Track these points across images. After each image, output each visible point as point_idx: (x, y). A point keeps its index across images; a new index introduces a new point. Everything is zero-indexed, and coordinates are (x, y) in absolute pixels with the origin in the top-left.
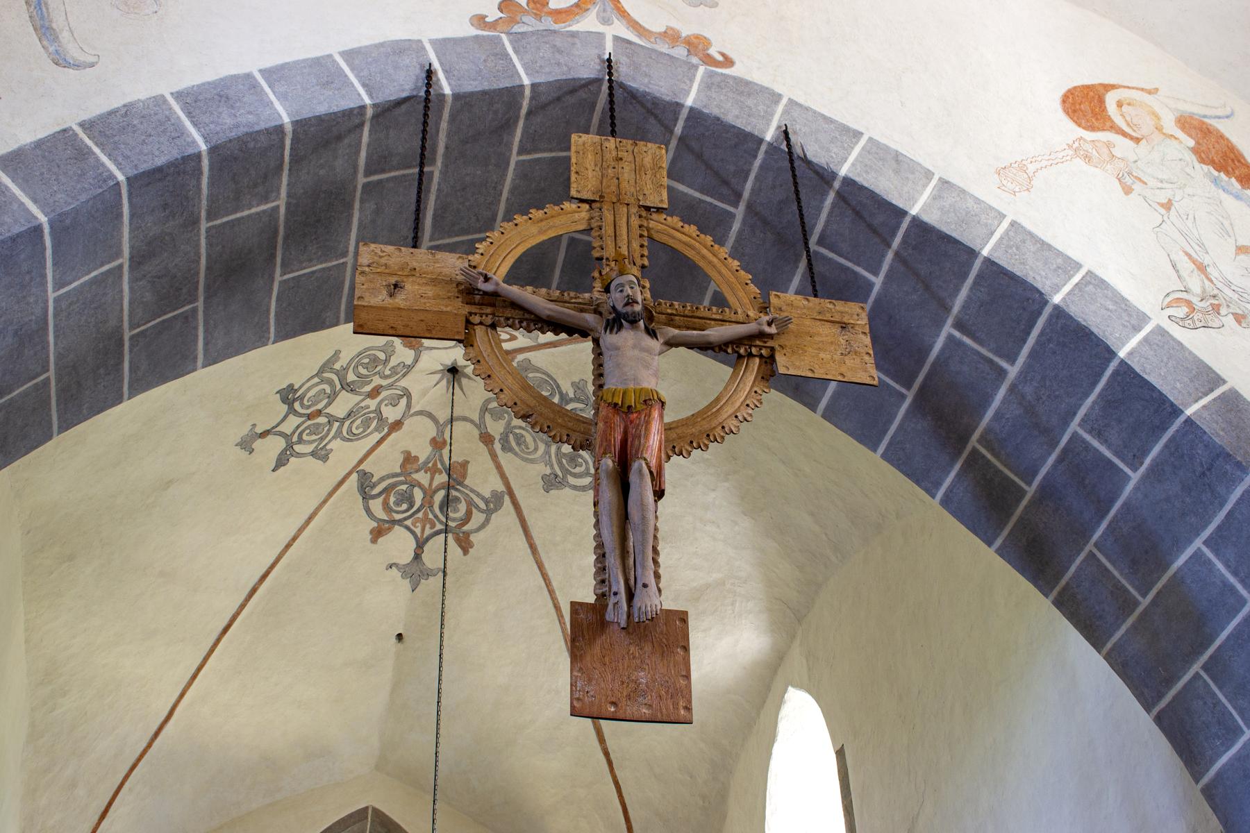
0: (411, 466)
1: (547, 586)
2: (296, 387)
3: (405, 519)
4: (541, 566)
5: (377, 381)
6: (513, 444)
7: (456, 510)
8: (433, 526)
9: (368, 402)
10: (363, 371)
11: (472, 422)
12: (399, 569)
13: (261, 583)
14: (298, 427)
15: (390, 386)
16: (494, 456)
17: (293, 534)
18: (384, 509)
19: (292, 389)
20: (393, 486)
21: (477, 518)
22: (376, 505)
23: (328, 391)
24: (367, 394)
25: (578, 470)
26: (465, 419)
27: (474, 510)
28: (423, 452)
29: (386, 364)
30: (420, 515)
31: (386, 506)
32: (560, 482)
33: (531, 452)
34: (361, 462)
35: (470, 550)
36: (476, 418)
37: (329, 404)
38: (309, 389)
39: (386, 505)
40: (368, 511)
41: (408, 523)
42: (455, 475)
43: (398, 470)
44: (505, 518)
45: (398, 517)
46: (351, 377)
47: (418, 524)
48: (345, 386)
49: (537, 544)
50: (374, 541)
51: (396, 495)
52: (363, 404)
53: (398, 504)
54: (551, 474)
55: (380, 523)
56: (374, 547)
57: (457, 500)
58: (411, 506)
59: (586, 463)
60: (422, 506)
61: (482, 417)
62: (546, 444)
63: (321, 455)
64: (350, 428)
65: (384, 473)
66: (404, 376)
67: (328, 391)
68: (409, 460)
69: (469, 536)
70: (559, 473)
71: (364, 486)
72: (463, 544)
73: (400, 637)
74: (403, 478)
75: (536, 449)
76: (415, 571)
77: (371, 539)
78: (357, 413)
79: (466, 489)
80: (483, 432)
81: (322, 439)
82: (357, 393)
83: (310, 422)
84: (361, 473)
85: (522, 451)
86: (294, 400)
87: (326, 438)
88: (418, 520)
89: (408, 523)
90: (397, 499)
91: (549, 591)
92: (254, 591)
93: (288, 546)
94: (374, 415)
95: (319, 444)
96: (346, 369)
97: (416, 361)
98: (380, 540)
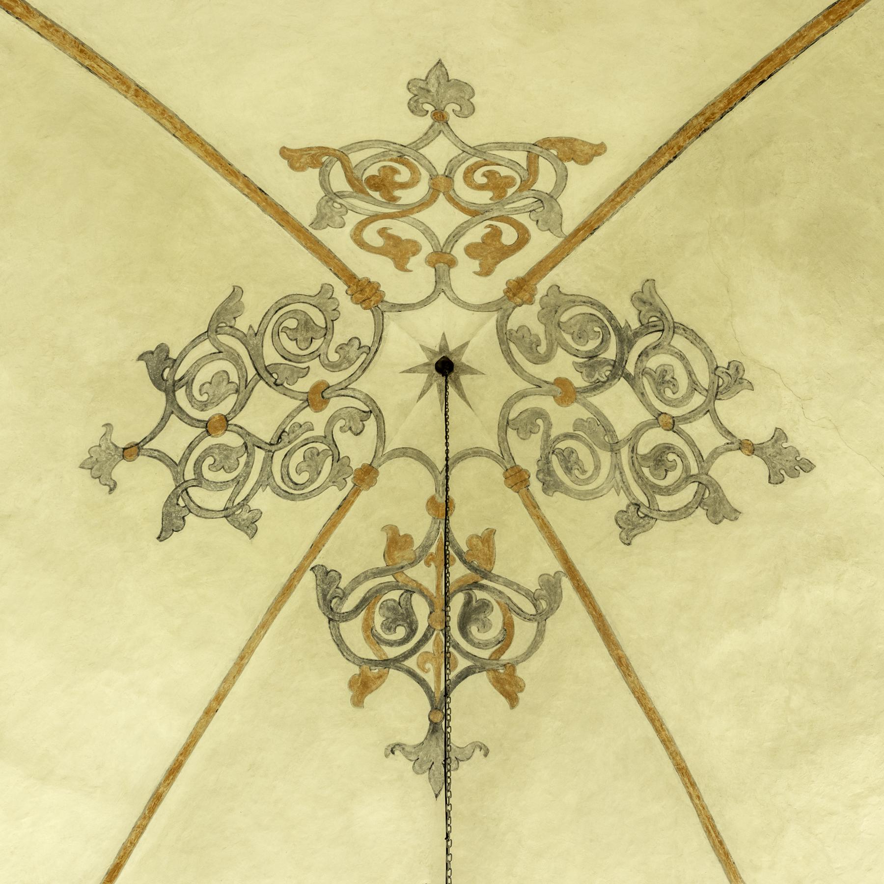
0: (400, 554)
1: (658, 731)
2: (174, 354)
3: (406, 656)
4: (641, 696)
5: (318, 374)
6: (560, 472)
7: (485, 626)
9: (307, 415)
10: (291, 347)
11: (488, 454)
12: (407, 755)
13: (169, 785)
14: (191, 448)
15: (343, 389)
16: (532, 506)
17: (215, 688)
18: (367, 638)
19: (167, 358)
21: (524, 631)
22: (352, 631)
24: (305, 397)
25: (673, 477)
26: (477, 452)
27: (516, 620)
29: (328, 337)
30: (429, 647)
31: (369, 633)
32: (646, 516)
33: (592, 476)
34: (316, 547)
35: (520, 695)
36: (494, 447)
37: (240, 406)
39: (369, 629)
40: (340, 643)
45: (393, 652)
47: (428, 666)
48: (265, 375)
49: (628, 655)
51: (385, 610)
52: (301, 418)
53: (389, 627)
54: (628, 506)
55: (365, 667)
56: (359, 713)
57: (485, 606)
58: (412, 632)
59: (681, 456)
60: (430, 629)
61: (503, 440)
62: (612, 451)
65: (358, 570)
66: (364, 368)
67: (234, 377)
68: (397, 543)
69: (514, 670)
70: (643, 499)
71: (328, 597)
72: (507, 687)
74: (389, 578)
75: (597, 468)
77: (352, 698)
78: (292, 436)
79: (496, 581)
80: (508, 466)
81: (239, 482)
82: (287, 392)
83: (209, 441)
84: (320, 573)
85: (576, 481)
87: (245, 480)
90: (387, 618)
91: (663, 741)
92: (157, 798)
93: (210, 712)
94: (324, 447)
95: (236, 494)
98: (368, 699)
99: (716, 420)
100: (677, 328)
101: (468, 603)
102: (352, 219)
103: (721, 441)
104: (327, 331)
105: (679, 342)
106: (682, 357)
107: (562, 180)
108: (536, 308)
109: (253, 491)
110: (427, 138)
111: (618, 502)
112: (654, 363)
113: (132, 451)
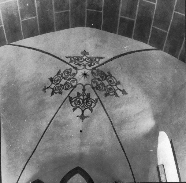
3: (79, 106)
5: (69, 77)
7: (89, 103)
8: (85, 108)
9: (68, 81)
10: (66, 75)
14: (54, 87)
16: (95, 91)
20: (76, 99)
21: (93, 105)
22: (73, 104)
23: (60, 79)
28: (81, 92)
30: (82, 105)
34: (69, 94)
37: (60, 82)
38: (55, 78)
39: (75, 104)
41: (80, 107)
42: (88, 96)
43: (77, 96)
44: (98, 104)
45: (78, 106)
46: (64, 76)
50: (74, 111)
52: (67, 82)
53: (77, 103)
56: (73, 112)
57: (89, 101)
58: (80, 103)
59: (113, 90)
61: (92, 84)
63: (60, 93)
64: (65, 87)
73: (81, 131)
75: (103, 88)
76: (82, 117)
81: (60, 89)
86: (53, 81)
88: (82, 106)
89: (80, 107)
96: (62, 74)
97: (77, 72)
99: (117, 87)
100: (112, 77)
101: (87, 101)
102: (74, 62)
103: (117, 89)
104: (71, 72)
105: (113, 78)
106: (113, 80)
107: (99, 60)
108: (96, 71)
109: (62, 90)
110: (83, 56)
111: (104, 92)
112: (110, 79)
113: (48, 88)
